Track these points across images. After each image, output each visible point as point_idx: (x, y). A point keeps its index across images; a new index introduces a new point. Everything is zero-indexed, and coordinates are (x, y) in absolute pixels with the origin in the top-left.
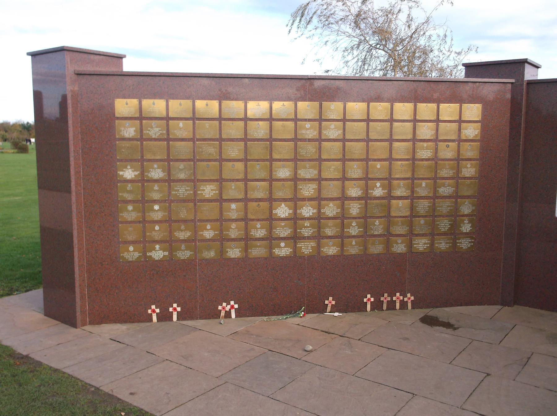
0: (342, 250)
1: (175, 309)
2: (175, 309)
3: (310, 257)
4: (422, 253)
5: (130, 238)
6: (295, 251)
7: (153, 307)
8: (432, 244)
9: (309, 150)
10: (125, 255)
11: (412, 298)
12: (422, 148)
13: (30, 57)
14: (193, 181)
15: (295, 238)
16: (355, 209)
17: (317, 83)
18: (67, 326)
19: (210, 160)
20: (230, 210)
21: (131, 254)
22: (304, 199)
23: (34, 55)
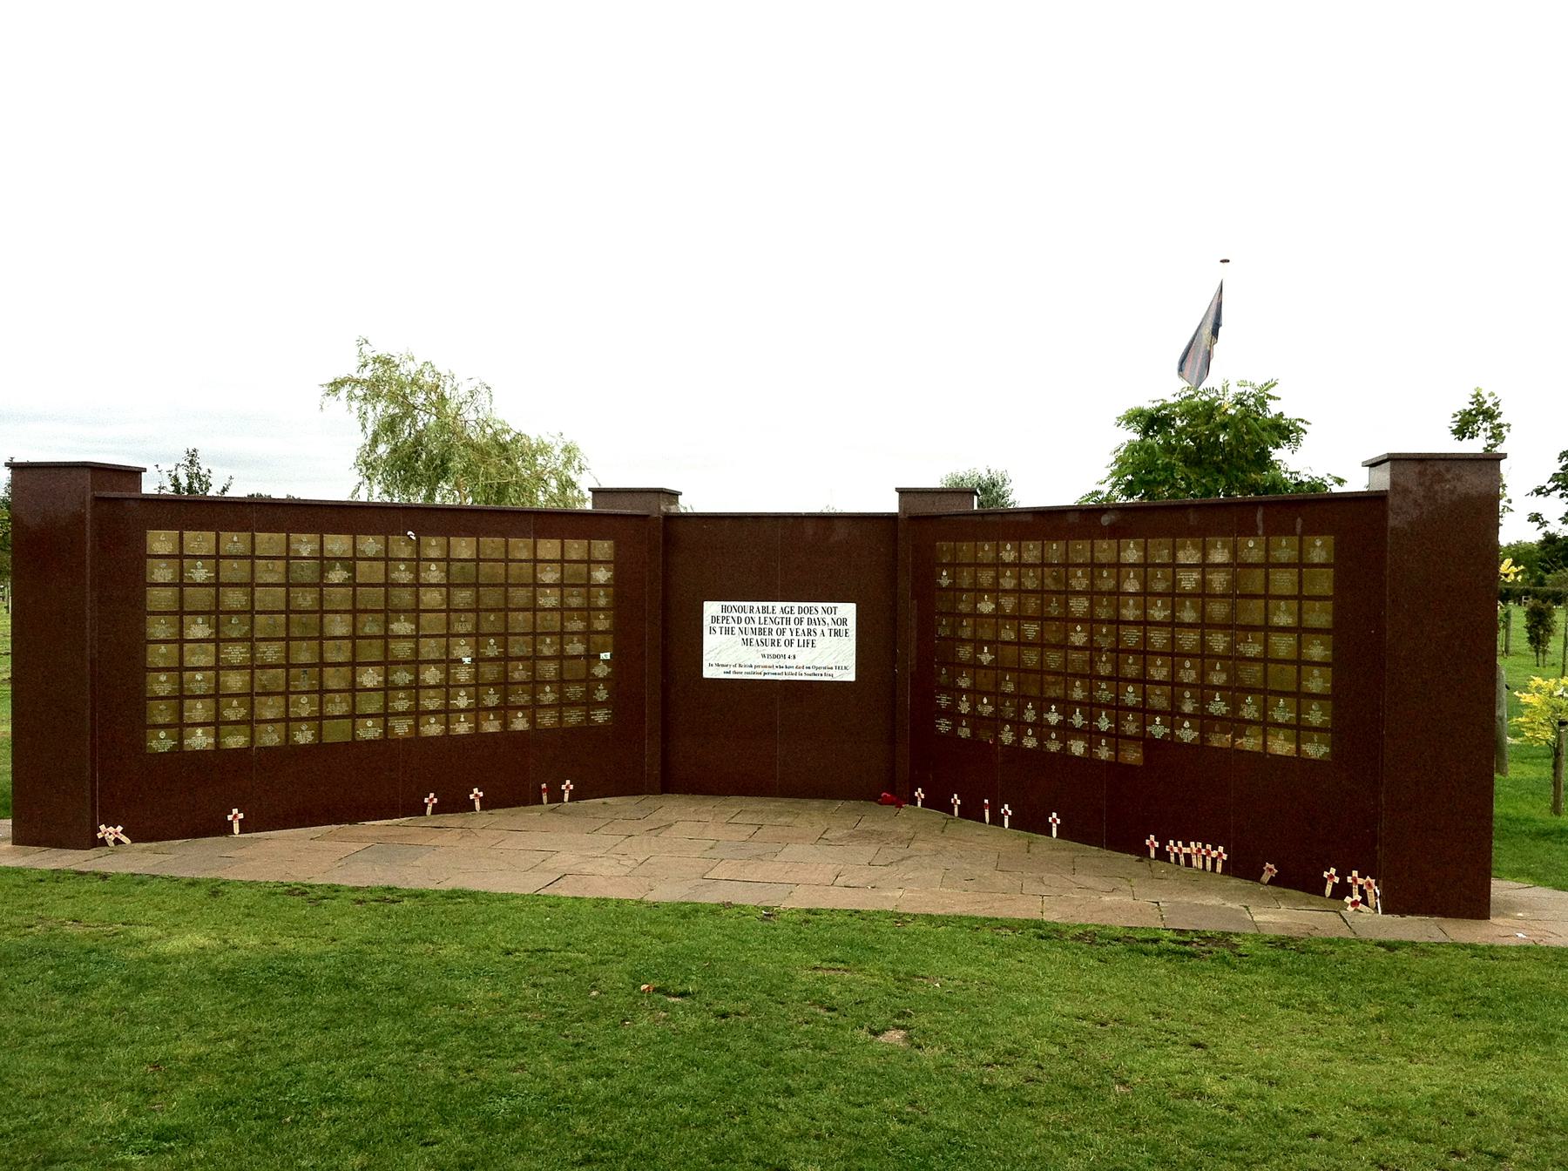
0: (447, 728)
1: (568, 786)
2: (568, 786)
3: (405, 740)
4: (547, 730)
5: (160, 720)
6: (217, 743)
7: (235, 811)
8: (561, 718)
9: (405, 597)
10: (154, 744)
11: (241, 816)
12: (545, 596)
13: (7, 473)
14: (250, 639)
15: (385, 715)
16: (549, 670)
17: (1011, 518)
18: (651, 801)
19: (273, 612)
20: (193, 680)
21: (161, 742)
22: (397, 663)
23: (15, 467)
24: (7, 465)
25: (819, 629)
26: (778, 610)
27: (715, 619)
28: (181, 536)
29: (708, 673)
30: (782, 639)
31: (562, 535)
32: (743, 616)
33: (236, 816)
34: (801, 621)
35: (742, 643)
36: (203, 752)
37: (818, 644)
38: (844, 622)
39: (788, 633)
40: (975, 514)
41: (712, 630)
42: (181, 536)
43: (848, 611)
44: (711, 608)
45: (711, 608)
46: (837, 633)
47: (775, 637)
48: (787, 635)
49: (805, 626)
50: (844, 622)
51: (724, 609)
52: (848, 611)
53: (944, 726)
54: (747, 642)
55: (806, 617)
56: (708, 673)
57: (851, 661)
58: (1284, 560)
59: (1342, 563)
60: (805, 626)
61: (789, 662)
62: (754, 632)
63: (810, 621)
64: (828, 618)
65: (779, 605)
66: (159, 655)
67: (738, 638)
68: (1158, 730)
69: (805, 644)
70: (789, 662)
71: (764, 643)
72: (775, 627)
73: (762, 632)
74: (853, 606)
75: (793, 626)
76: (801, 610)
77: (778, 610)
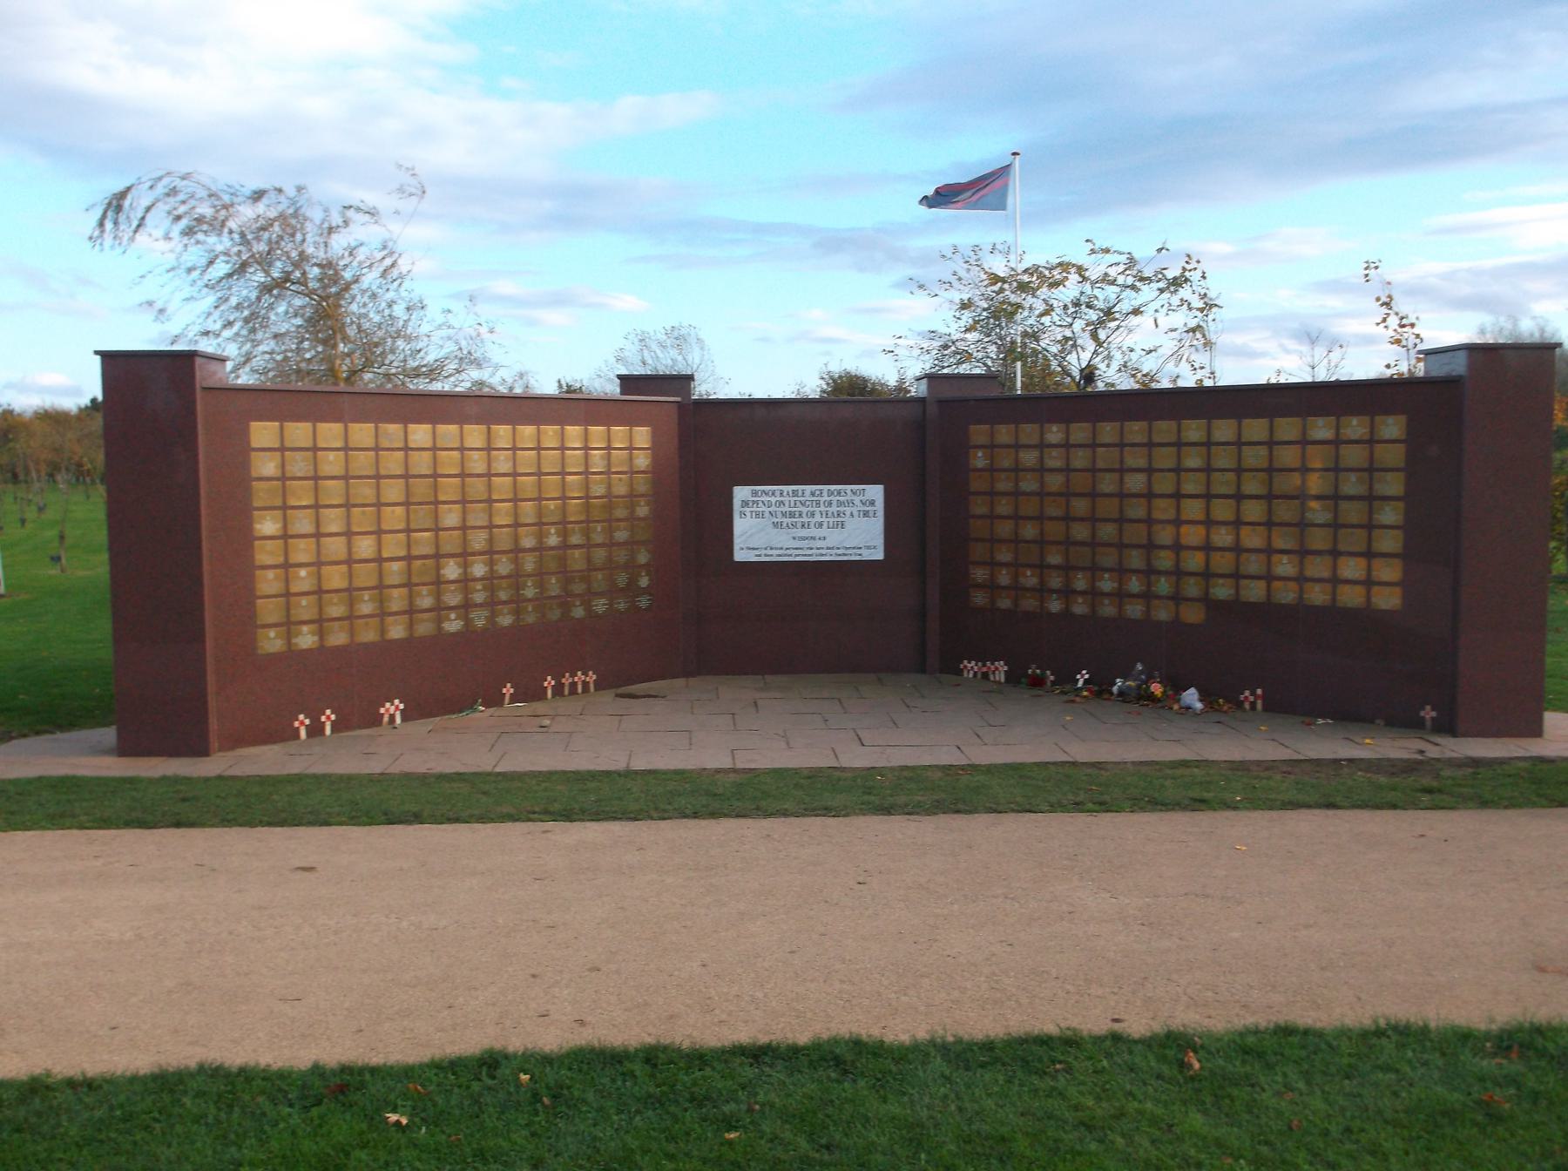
11: (307, 722)
13: (98, 358)
24: (97, 353)
25: (848, 510)
26: (807, 493)
27: (745, 504)
28: (282, 428)
29: (739, 556)
30: (813, 521)
31: (282, 417)
32: (773, 499)
33: (393, 708)
34: (830, 504)
35: (770, 525)
36: (309, 650)
37: (845, 524)
38: (872, 503)
39: (818, 516)
40: (1019, 398)
41: (743, 514)
42: (282, 428)
43: (876, 492)
44: (741, 493)
45: (741, 493)
46: (866, 514)
47: (805, 519)
48: (818, 518)
49: (834, 509)
50: (872, 503)
51: (755, 493)
52: (876, 492)
53: (979, 599)
54: (775, 525)
55: (834, 499)
56: (739, 556)
57: (878, 540)
58: (1354, 437)
59: (1414, 441)
60: (834, 509)
61: (819, 544)
62: (784, 514)
63: (840, 504)
64: (857, 500)
65: (809, 488)
66: (266, 554)
67: (767, 522)
68: (1222, 591)
69: (836, 525)
70: (819, 544)
71: (794, 525)
72: (804, 510)
73: (792, 515)
74: (737, 490)
75: (822, 508)
76: (830, 493)
77: (807, 493)
